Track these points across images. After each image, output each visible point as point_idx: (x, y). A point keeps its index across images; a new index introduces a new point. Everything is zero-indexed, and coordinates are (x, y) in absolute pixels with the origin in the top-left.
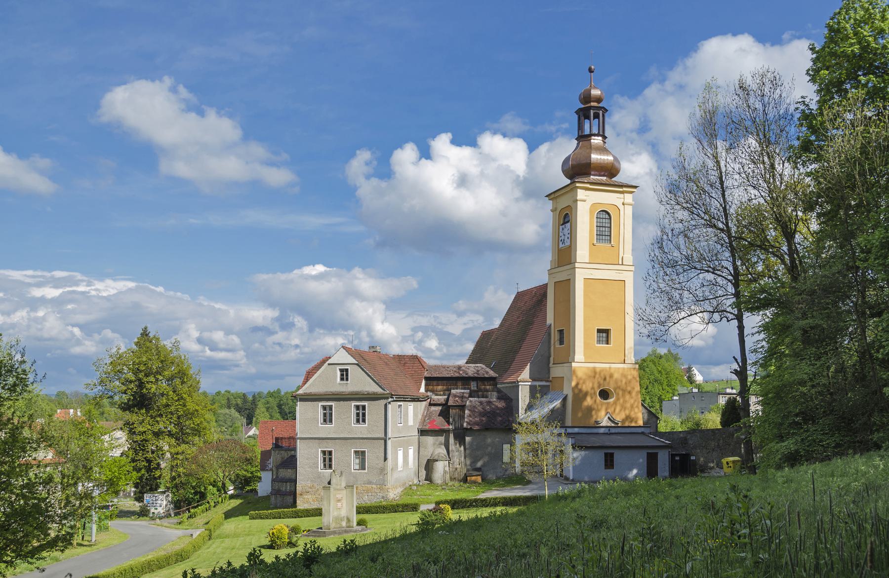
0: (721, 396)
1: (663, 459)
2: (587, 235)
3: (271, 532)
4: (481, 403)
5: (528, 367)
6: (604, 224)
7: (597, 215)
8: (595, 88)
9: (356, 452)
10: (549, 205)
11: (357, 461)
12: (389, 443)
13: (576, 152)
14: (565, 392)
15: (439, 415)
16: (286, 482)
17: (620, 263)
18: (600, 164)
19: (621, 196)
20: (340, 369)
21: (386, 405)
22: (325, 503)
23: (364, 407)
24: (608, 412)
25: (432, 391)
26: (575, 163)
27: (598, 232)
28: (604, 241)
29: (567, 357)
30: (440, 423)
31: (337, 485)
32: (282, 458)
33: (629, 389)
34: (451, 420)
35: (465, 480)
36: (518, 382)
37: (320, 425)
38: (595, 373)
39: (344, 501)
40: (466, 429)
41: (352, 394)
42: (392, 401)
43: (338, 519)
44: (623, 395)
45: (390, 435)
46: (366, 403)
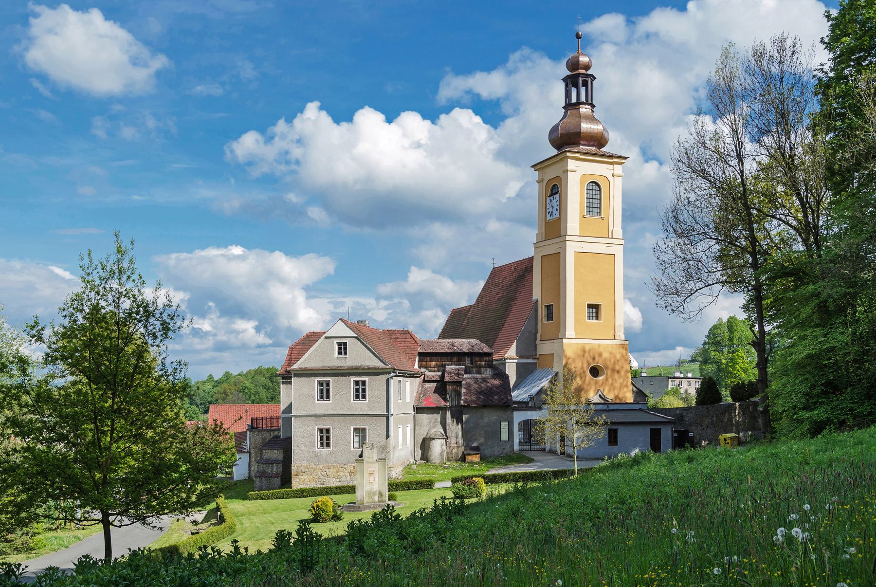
0: (670, 380)
1: (667, 434)
5: (515, 344)
6: (594, 196)
8: (583, 55)
9: (355, 430)
11: (357, 439)
12: (391, 419)
13: (564, 120)
17: (610, 236)
18: (590, 133)
19: (611, 167)
21: (388, 381)
22: (358, 476)
23: (364, 383)
25: (426, 367)
26: (563, 132)
28: (594, 213)
29: (558, 334)
30: (436, 400)
31: (369, 458)
32: (263, 439)
33: (617, 368)
34: (448, 397)
36: (505, 359)
38: (584, 351)
39: (376, 475)
40: (464, 406)
41: (351, 368)
42: (394, 376)
43: (371, 494)
45: (392, 411)
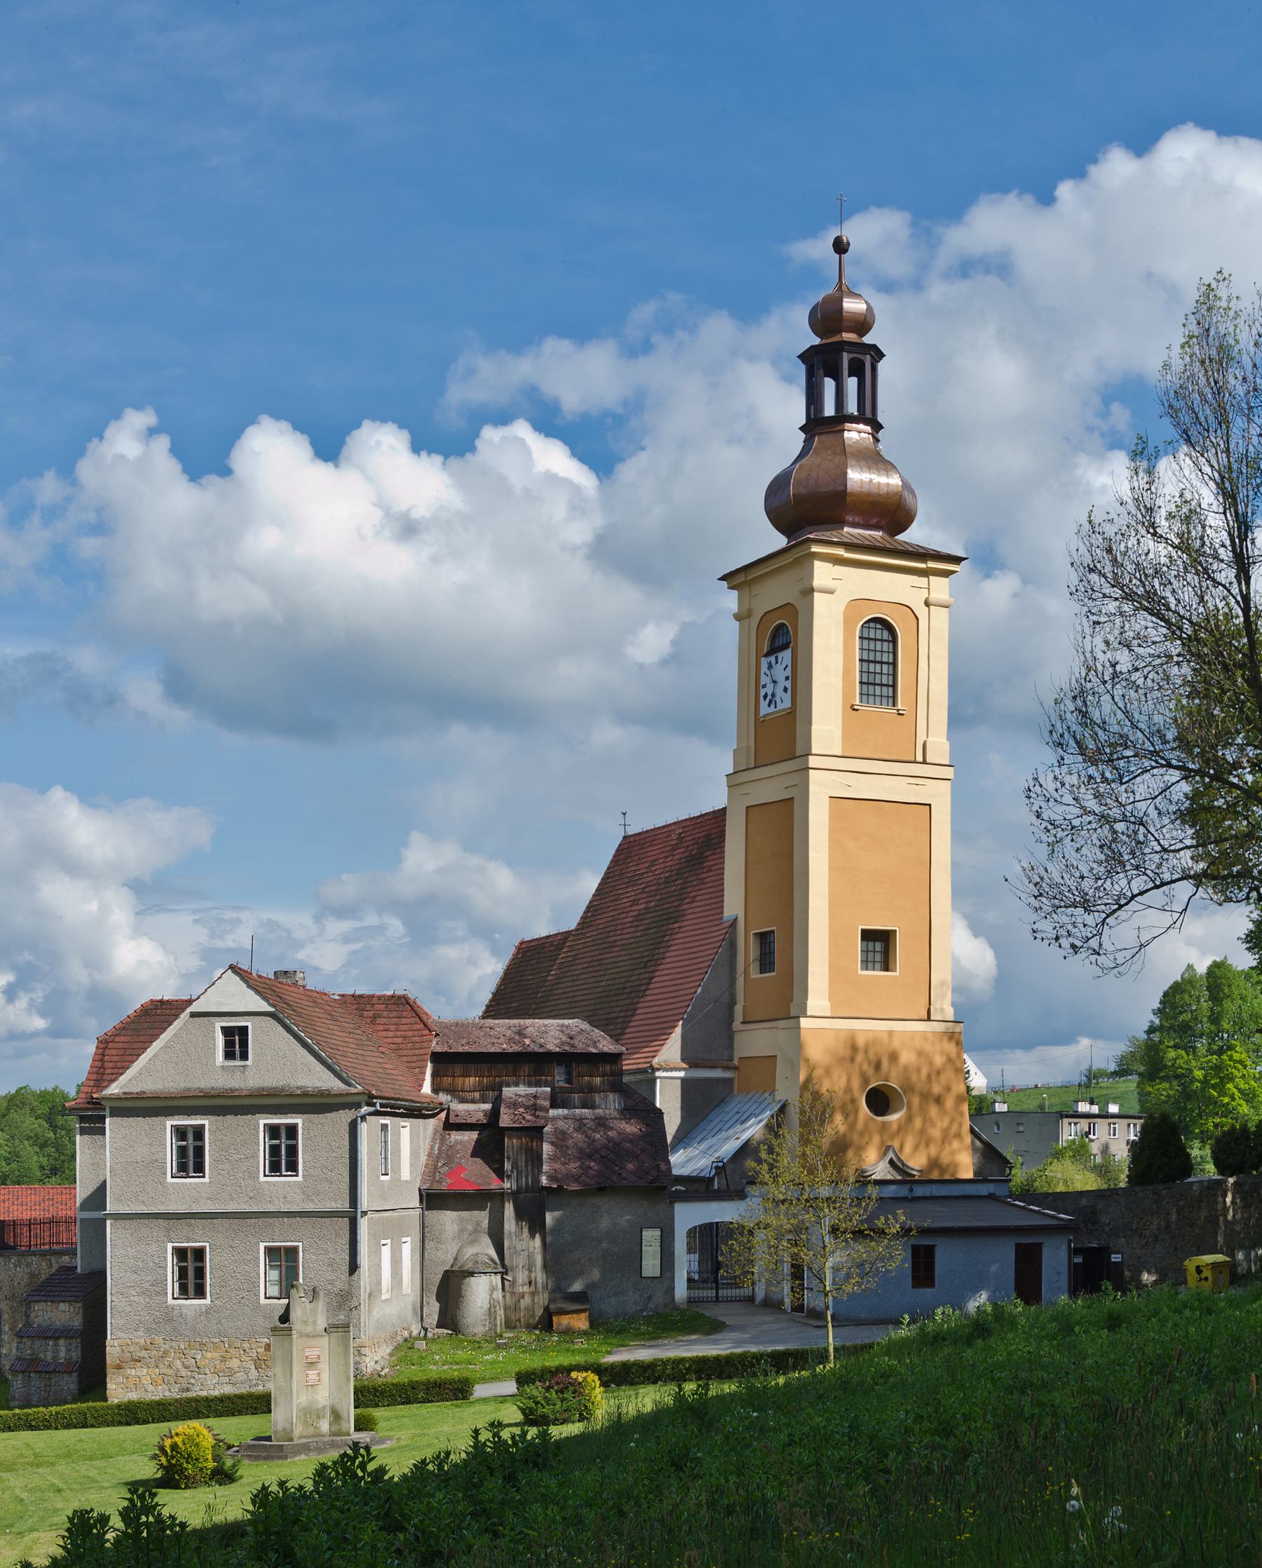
0: (1066, 1121)
2: (838, 682)
3: (168, 1443)
4: (580, 1121)
5: (678, 1031)
6: (878, 654)
7: (862, 631)
10: (730, 600)
11: (274, 1275)
12: (363, 1225)
13: (804, 461)
14: (781, 1095)
15: (474, 1154)
16: (57, 1338)
17: (920, 758)
18: (869, 495)
19: (922, 581)
20: (222, 1028)
24: (888, 1148)
25: (451, 1091)
26: (802, 490)
27: (865, 675)
28: (878, 699)
30: (478, 1174)
31: (305, 1322)
32: (32, 1275)
33: (936, 1089)
35: (546, 1323)
36: (654, 1070)
37: (169, 1179)
38: (854, 1048)
39: (324, 1366)
41: (252, 1095)
42: (371, 1114)
43: (310, 1414)
44: (923, 1110)
45: (364, 1203)
46: (298, 1120)
